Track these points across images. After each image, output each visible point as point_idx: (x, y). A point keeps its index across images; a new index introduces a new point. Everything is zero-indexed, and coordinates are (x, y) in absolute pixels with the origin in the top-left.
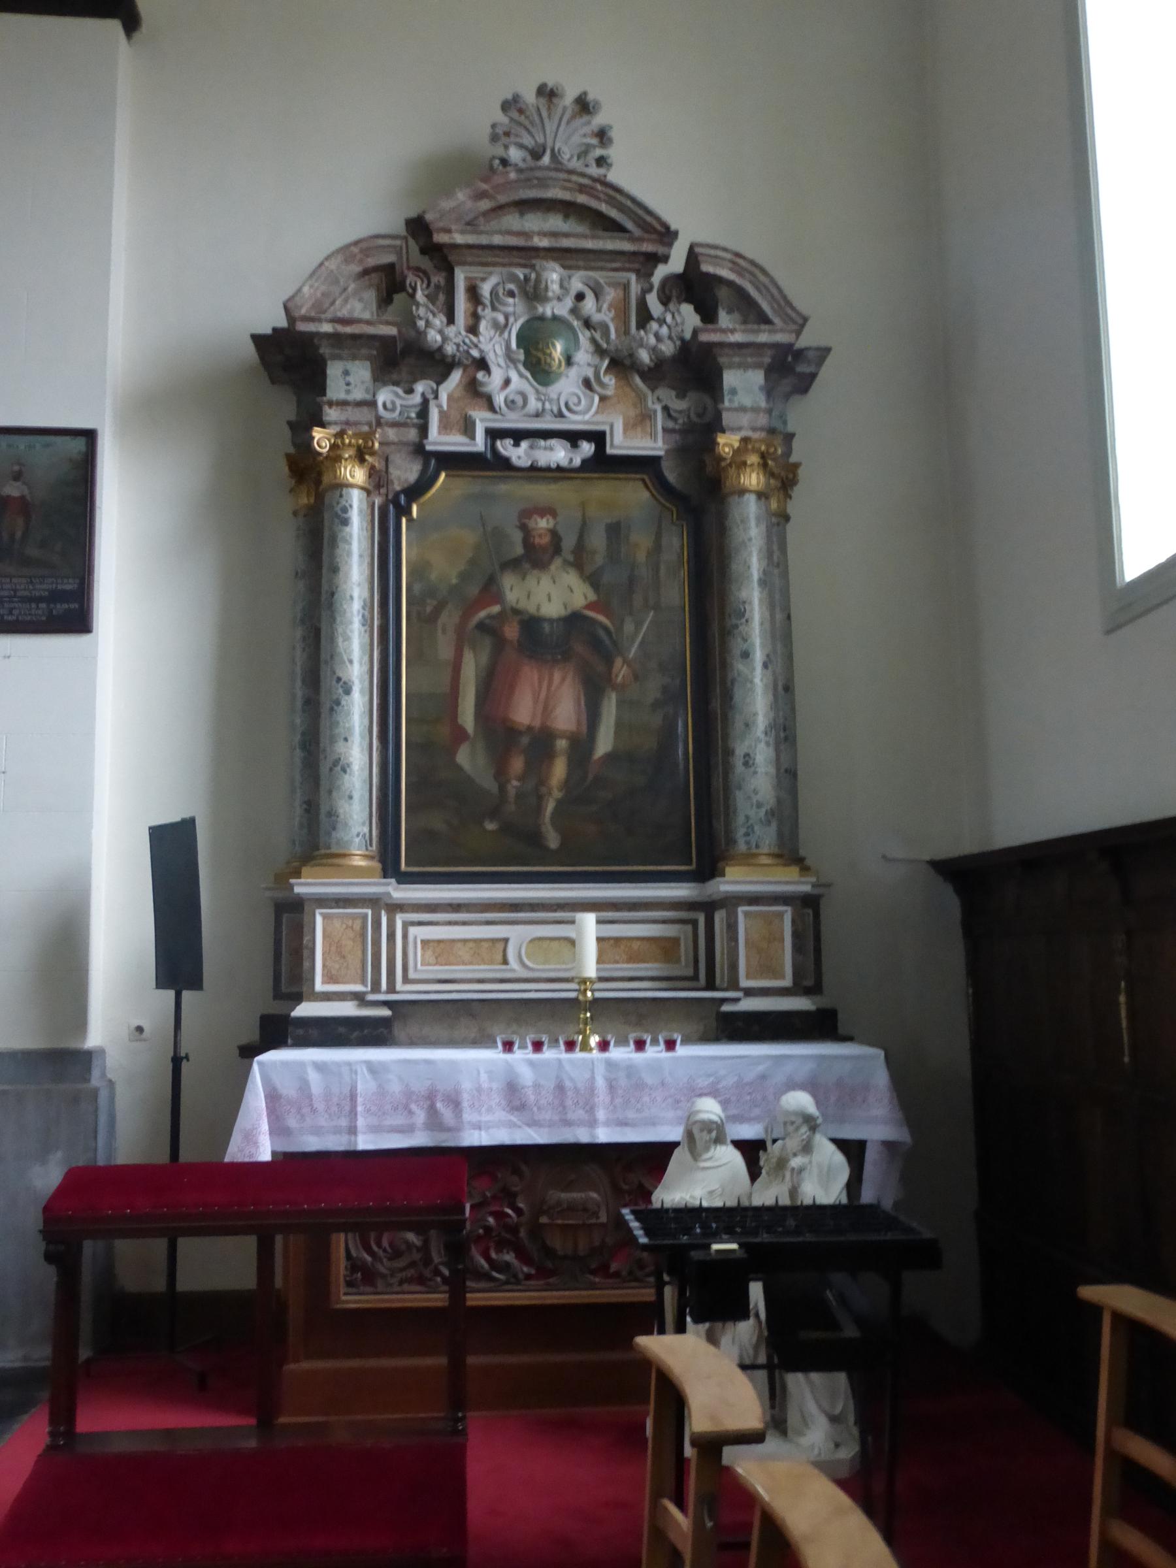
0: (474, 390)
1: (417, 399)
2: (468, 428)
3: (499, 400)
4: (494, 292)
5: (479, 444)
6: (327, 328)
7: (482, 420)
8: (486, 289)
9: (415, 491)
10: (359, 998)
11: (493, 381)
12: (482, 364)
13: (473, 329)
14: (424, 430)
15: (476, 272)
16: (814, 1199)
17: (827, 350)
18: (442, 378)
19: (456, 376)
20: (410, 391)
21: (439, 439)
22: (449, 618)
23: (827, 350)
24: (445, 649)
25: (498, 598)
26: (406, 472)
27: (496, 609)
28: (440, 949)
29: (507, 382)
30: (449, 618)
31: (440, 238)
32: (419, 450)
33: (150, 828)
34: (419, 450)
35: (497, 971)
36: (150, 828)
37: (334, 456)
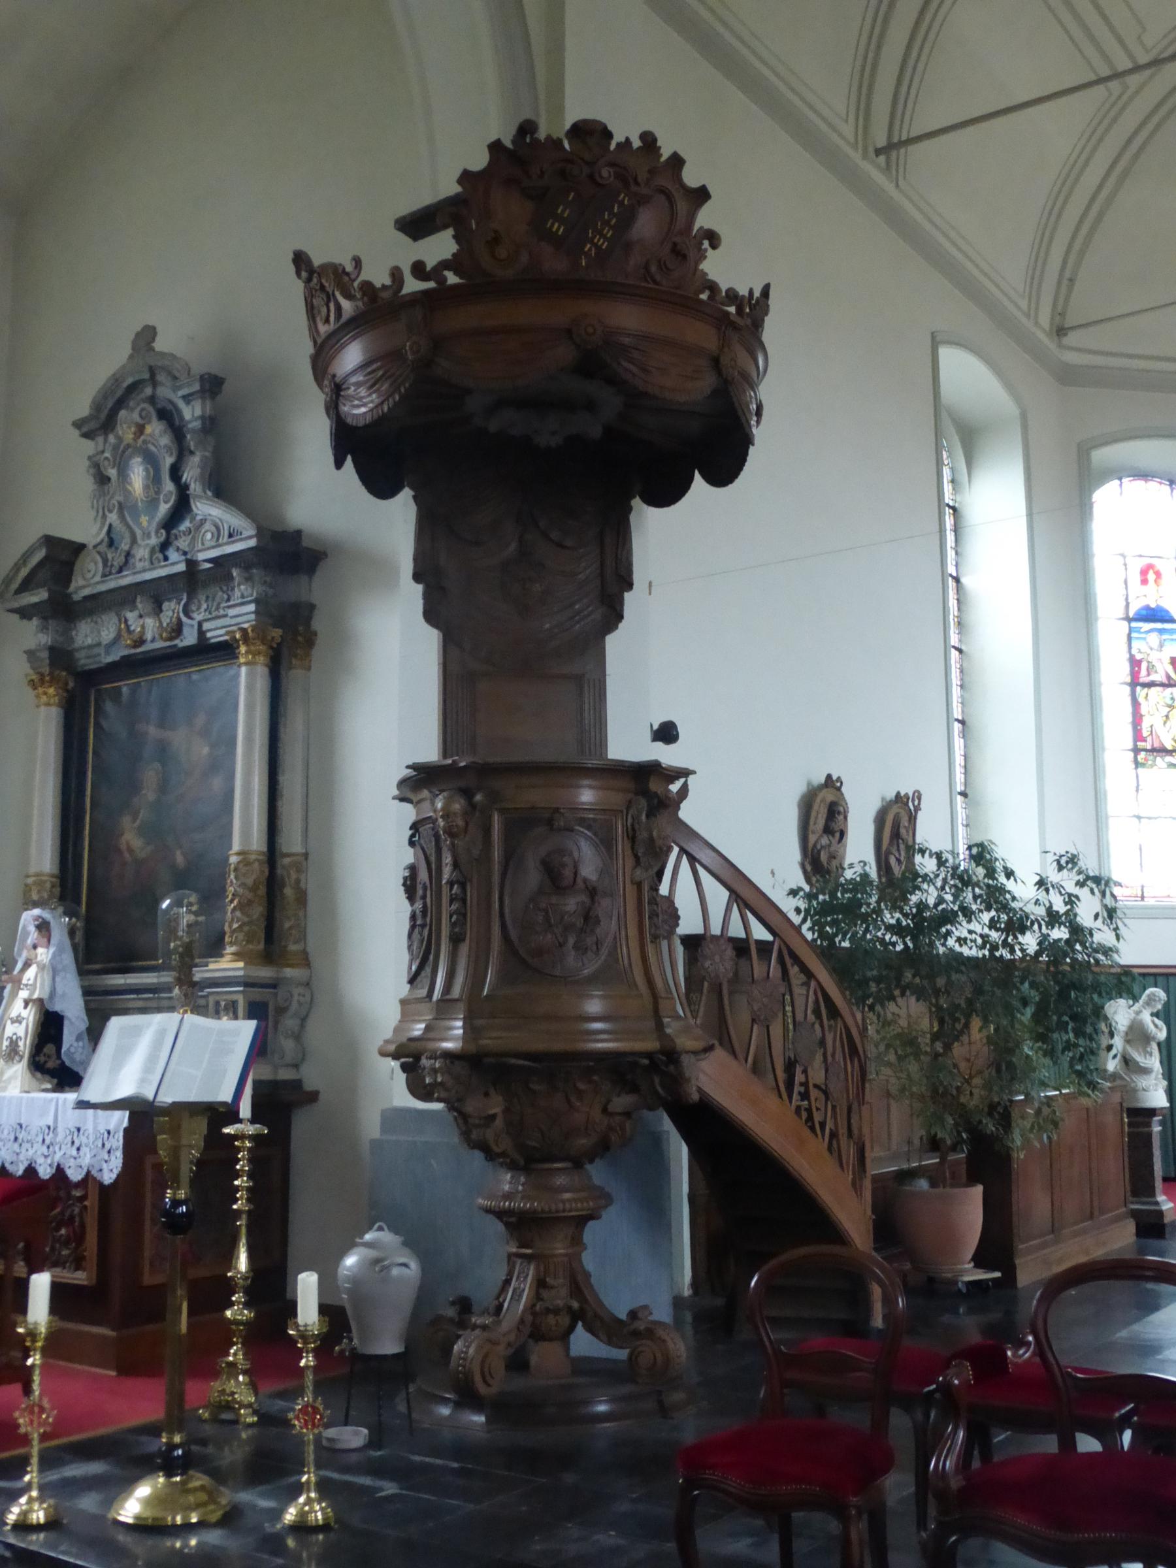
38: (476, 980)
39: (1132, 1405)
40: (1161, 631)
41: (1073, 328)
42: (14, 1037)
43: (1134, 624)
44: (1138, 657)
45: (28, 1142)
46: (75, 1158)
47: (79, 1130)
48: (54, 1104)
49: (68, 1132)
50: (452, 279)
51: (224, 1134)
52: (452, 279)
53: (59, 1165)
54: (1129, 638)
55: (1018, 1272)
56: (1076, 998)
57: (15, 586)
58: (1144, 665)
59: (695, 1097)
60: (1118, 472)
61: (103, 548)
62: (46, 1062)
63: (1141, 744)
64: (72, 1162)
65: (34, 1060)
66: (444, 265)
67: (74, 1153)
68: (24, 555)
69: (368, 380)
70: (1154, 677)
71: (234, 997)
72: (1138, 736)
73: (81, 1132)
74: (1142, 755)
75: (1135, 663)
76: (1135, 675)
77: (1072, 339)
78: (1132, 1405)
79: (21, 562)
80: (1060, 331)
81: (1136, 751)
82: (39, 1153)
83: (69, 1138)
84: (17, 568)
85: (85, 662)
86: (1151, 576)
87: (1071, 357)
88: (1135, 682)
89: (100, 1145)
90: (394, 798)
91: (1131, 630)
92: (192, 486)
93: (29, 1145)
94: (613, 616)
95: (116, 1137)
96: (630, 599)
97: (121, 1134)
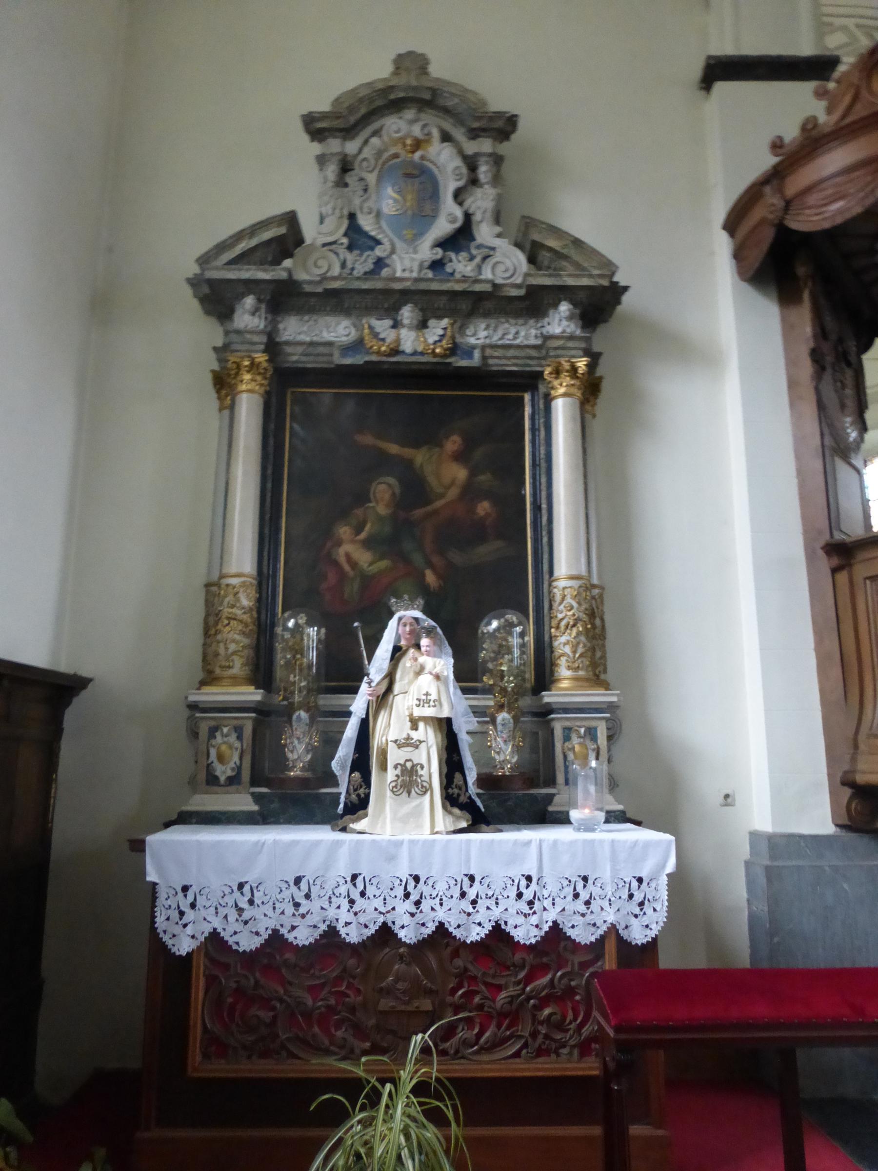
39: (311, 1109)
42: (409, 765)
45: (488, 897)
46: (583, 915)
47: (585, 879)
48: (533, 850)
49: (452, 882)
53: (440, 922)
55: (857, 965)
56: (313, 702)
62: (459, 795)
64: (578, 920)
65: (447, 793)
67: (582, 908)
68: (254, 225)
69: (802, 209)
71: (593, 724)
73: (590, 882)
78: (311, 1109)
79: (249, 231)
82: (512, 911)
83: (569, 891)
84: (239, 236)
85: (294, 357)
89: (625, 896)
93: (491, 903)
95: (653, 885)
97: (664, 880)
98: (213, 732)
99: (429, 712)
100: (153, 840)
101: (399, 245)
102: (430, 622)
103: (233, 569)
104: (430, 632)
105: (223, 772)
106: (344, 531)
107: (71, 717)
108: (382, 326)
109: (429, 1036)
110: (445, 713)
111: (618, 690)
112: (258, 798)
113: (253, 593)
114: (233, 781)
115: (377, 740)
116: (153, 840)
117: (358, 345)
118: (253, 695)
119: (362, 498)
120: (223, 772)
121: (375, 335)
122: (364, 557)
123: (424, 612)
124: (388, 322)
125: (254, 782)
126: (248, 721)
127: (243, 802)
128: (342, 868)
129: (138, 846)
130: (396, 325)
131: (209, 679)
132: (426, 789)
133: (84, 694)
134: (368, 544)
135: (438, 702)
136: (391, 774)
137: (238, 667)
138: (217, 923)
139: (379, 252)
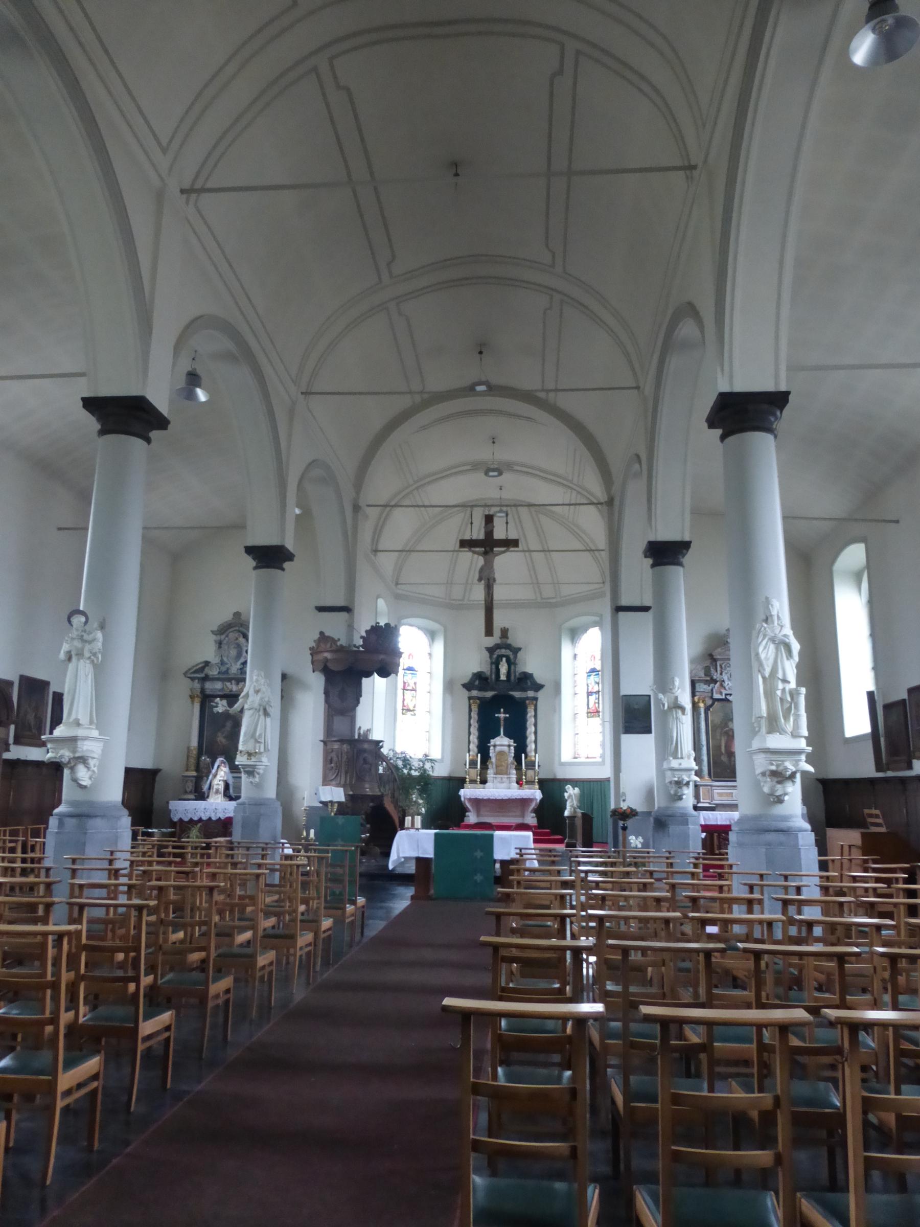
0: (722, 685)
1: (710, 688)
2: (721, 693)
3: (727, 688)
4: (725, 666)
5: (723, 697)
6: (697, 678)
7: (724, 692)
8: (723, 666)
9: (711, 706)
10: (709, 803)
11: (725, 685)
12: (723, 681)
13: (721, 674)
14: (712, 694)
15: (722, 662)
16: (816, 885)
17: (486, 648)
18: (715, 684)
19: (718, 683)
20: (709, 686)
21: (716, 696)
22: (719, 731)
23: (486, 648)
24: (718, 737)
25: (728, 727)
26: (709, 702)
27: (727, 729)
28: (720, 794)
29: (728, 684)
30: (719, 731)
31: (715, 657)
32: (712, 697)
33: (709, 428)
34: (712, 697)
35: (730, 798)
36: (709, 428)
37: (698, 702)
38: (351, 781)
40: (412, 674)
41: (380, 551)
43: (406, 671)
44: (406, 681)
50: (361, 649)
51: (815, 770)
52: (361, 649)
54: (404, 675)
57: (191, 671)
58: (407, 684)
59: (576, 788)
60: (405, 624)
61: (219, 665)
63: (404, 708)
66: (360, 646)
70: (409, 688)
72: (404, 706)
74: (404, 711)
75: (405, 683)
76: (404, 686)
77: (399, 586)
80: (397, 584)
81: (403, 710)
85: (208, 692)
86: (411, 657)
87: (400, 592)
88: (404, 689)
90: (321, 741)
91: (405, 673)
92: (838, 931)
94: (358, 702)
96: (361, 699)
98: (186, 782)
99: (222, 779)
100: (171, 802)
101: (233, 664)
102: (225, 760)
103: (192, 745)
104: (224, 763)
105: (188, 790)
106: (219, 734)
107: (158, 778)
108: (228, 684)
109: (473, 1078)
110: (225, 779)
111: (521, 756)
112: (195, 796)
113: (197, 750)
114: (191, 792)
115: (213, 783)
116: (171, 802)
117: (222, 689)
118: (194, 774)
119: (224, 726)
120: (188, 790)
121: (227, 687)
122: (224, 741)
123: (225, 759)
124: (229, 683)
125: (195, 792)
126: (194, 779)
127: (192, 797)
128: (203, 807)
129: (168, 803)
130: (231, 684)
131: (187, 770)
132: (220, 793)
133: (159, 774)
134: (225, 737)
135: (224, 777)
136: (214, 790)
137: (193, 768)
138: (181, 816)
139: (227, 666)
